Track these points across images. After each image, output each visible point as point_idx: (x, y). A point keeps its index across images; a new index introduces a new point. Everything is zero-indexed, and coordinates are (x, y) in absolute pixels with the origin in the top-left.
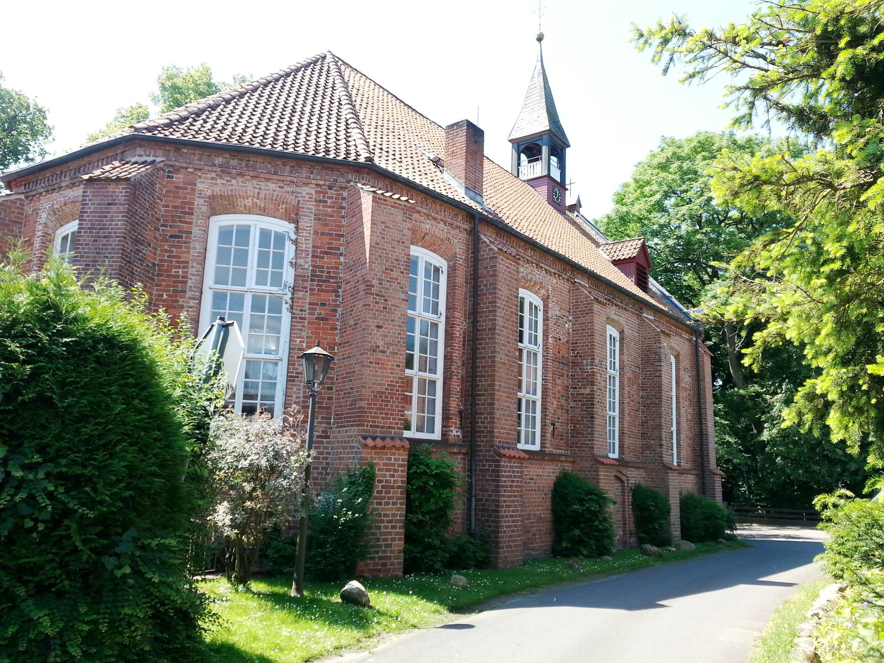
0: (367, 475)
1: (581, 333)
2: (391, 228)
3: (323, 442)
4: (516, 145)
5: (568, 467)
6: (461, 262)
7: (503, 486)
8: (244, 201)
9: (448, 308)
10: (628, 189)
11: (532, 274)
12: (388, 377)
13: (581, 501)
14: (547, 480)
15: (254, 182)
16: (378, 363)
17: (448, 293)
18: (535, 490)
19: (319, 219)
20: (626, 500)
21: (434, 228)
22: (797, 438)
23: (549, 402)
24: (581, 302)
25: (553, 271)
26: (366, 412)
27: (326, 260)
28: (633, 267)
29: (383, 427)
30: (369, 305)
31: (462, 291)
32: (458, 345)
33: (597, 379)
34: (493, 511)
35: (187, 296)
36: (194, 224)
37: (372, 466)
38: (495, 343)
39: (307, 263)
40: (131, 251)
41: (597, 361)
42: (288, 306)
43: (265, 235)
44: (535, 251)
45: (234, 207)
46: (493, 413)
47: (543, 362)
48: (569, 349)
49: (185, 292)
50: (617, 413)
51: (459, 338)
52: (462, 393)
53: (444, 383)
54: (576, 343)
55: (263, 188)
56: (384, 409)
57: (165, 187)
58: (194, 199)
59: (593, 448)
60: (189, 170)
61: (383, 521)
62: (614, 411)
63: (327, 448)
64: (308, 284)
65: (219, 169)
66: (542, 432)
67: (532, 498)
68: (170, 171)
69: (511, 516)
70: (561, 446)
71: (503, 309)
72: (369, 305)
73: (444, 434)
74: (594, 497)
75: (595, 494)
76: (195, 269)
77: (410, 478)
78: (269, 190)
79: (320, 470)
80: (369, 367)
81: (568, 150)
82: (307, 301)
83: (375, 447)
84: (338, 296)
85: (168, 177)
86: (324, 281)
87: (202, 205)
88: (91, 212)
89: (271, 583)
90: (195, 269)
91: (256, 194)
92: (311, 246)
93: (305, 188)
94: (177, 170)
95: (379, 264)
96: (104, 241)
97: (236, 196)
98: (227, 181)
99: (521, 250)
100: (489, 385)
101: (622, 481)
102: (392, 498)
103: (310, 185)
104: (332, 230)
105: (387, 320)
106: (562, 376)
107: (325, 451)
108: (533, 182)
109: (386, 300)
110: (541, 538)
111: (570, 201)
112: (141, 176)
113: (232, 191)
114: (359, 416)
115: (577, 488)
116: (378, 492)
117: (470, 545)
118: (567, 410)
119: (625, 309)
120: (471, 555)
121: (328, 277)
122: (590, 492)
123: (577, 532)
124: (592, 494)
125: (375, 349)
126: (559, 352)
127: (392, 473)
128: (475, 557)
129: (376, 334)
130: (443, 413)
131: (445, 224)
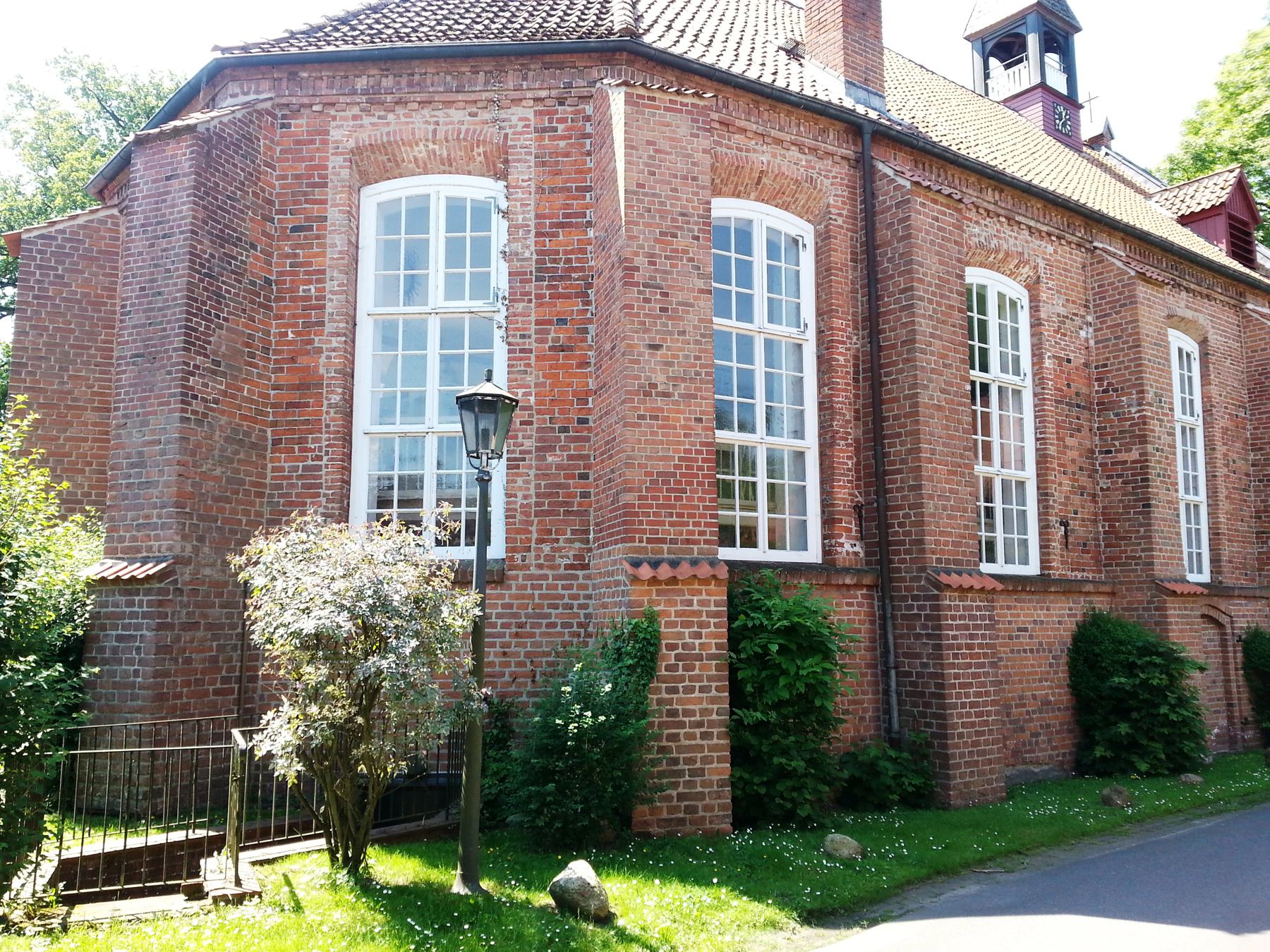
0: (641, 635)
1: (1114, 345)
2: (667, 153)
3: (576, 577)
4: (979, 44)
5: (1102, 604)
6: (840, 221)
7: (951, 647)
8: (413, 151)
9: (819, 313)
10: (1207, 110)
11: (999, 238)
12: (679, 443)
13: (1131, 669)
14: (1058, 629)
15: (426, 112)
16: (656, 418)
17: (818, 285)
18: (1031, 651)
19: (544, 164)
20: (1231, 660)
21: (778, 160)
22: (22, 713)
23: (1053, 482)
24: (1109, 284)
25: (1045, 228)
26: (636, 514)
27: (561, 238)
28: (1221, 223)
29: (673, 541)
30: (632, 307)
31: (846, 278)
32: (843, 378)
33: (1153, 431)
34: (933, 695)
35: (326, 331)
36: (330, 203)
37: (652, 618)
38: (915, 368)
39: (528, 247)
40: (212, 256)
41: (1150, 396)
42: (502, 332)
43: (455, 209)
44: (1001, 191)
45: (398, 165)
46: (921, 506)
47: (1035, 406)
48: (1089, 379)
49: (322, 324)
50: (1202, 497)
51: (846, 366)
52: (857, 471)
53: (822, 454)
54: (1105, 366)
55: (441, 120)
56: (674, 507)
57: (278, 144)
58: (327, 159)
59: (1152, 564)
60: (315, 108)
61: (682, 725)
62: (1196, 494)
63: (585, 587)
64: (531, 287)
65: (364, 98)
66: (1041, 540)
67: (1026, 666)
68: (284, 117)
69: (973, 705)
70: (1083, 564)
71: (930, 302)
72: (632, 307)
73: (826, 552)
74: (1158, 660)
75: (1159, 655)
76: (336, 283)
77: (735, 639)
78: (452, 123)
79: (575, 629)
80: (639, 425)
81: (1077, 38)
82: (533, 318)
83: (654, 581)
84: (588, 303)
85: (283, 126)
86: (562, 278)
87: (341, 167)
88: (144, 198)
89: (432, 861)
90: (336, 283)
91: (430, 136)
92: (532, 215)
93: (514, 109)
94: (296, 112)
95: (647, 225)
96: (164, 243)
97: (396, 142)
98: (379, 118)
99: (970, 192)
100: (909, 452)
101: (1220, 625)
102: (699, 678)
103: (524, 103)
104: (567, 181)
105: (671, 333)
106: (1079, 431)
107: (582, 593)
108: (1014, 102)
109: (666, 295)
110: (1050, 741)
111: (1088, 130)
112: (221, 123)
113: (388, 134)
114: (624, 523)
115: (1121, 643)
116: (668, 668)
117: (888, 765)
118: (1094, 496)
119: (1208, 296)
120: (889, 782)
121: (566, 270)
122: (1147, 650)
123: (1124, 728)
124: (1151, 654)
125: (649, 390)
126: (1069, 386)
127: (696, 629)
128: (901, 785)
129: (648, 362)
130: (823, 512)
131: (801, 151)
